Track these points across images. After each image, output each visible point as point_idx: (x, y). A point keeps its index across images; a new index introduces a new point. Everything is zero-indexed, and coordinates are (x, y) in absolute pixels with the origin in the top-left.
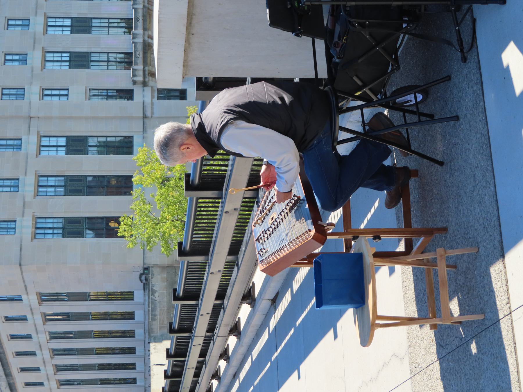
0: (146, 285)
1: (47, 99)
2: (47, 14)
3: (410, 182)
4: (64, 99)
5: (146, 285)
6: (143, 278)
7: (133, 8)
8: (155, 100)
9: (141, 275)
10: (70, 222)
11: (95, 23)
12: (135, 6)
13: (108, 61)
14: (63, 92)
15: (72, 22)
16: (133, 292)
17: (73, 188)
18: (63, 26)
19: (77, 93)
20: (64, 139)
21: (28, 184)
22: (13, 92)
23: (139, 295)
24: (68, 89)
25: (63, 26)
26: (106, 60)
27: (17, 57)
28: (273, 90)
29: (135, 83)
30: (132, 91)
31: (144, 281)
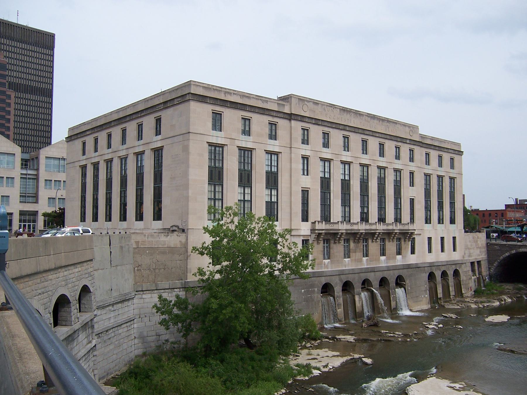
0: (171, 230)
1: (301, 161)
2: (226, 146)
3: (378, 380)
4: (301, 173)
5: (171, 230)
6: (174, 228)
7: (315, 221)
8: (302, 238)
9: (178, 227)
10: (219, 172)
11: (247, 190)
12: (317, 222)
13: (215, 200)
14: (306, 171)
15: (347, 180)
16: (142, 220)
17: (243, 175)
18: (215, 160)
19: (306, 182)
20: (276, 170)
21: (247, 142)
22: (306, 138)
23: (158, 224)
24: (308, 175)
25: (215, 160)
26: (217, 198)
27: (306, 138)
28: (511, 288)
29: (314, 223)
30: (307, 221)
31: (171, 229)
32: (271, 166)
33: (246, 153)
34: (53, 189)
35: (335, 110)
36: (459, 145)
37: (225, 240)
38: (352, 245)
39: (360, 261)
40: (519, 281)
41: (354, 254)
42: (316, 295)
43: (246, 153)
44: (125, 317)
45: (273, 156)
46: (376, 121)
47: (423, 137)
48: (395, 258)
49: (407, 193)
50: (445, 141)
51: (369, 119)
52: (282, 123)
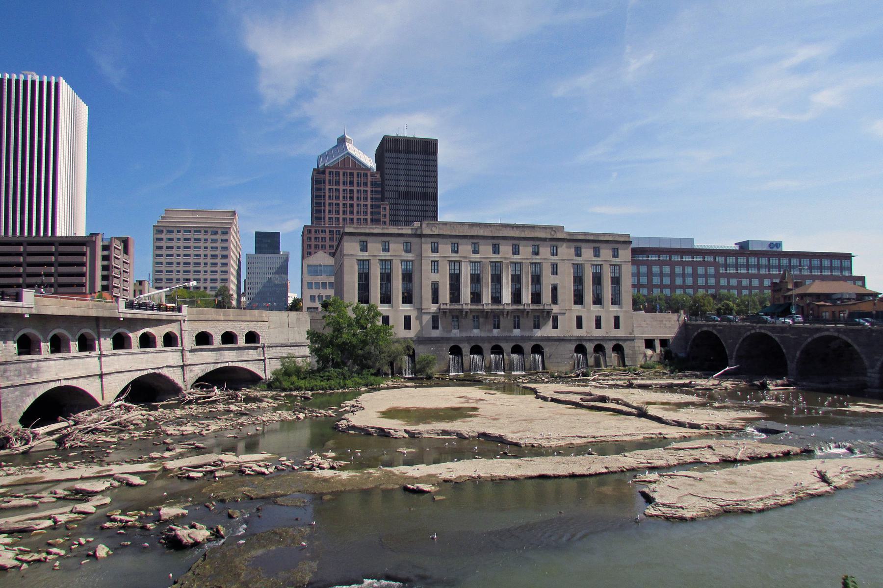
19: (435, 277)
39: (491, 331)
49: (548, 280)
52: (414, 240)
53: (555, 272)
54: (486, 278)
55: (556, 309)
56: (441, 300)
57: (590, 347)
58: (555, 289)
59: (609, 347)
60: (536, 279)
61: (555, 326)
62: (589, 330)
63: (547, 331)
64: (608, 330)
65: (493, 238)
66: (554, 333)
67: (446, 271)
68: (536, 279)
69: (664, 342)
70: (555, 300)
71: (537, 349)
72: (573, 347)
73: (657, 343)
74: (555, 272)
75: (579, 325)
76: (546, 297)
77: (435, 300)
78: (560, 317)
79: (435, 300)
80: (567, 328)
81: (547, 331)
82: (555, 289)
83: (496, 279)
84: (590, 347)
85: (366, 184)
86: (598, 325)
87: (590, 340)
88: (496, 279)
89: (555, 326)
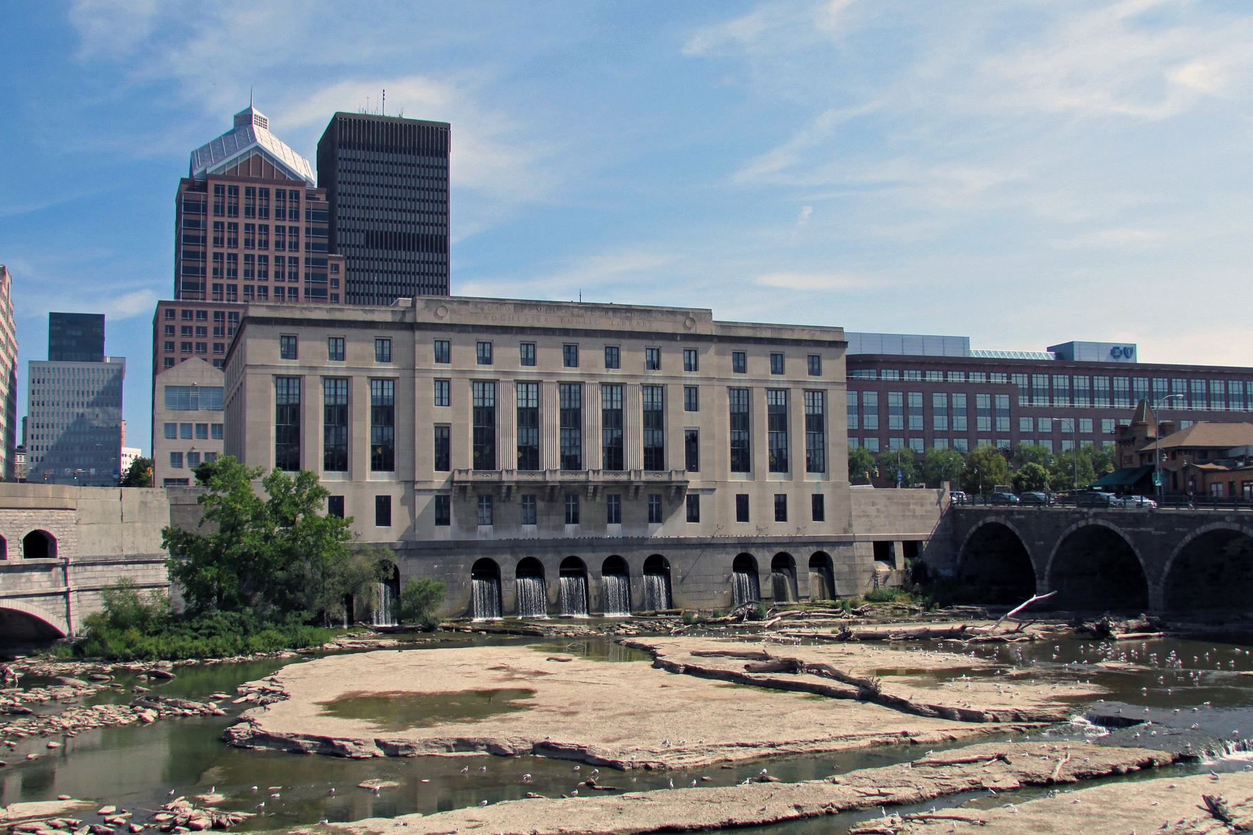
19: (443, 415)
32: (484, 398)
33: (572, 391)
34: (179, 436)
35: (504, 308)
36: (840, 330)
37: (1089, 443)
38: (540, 505)
39: (561, 528)
40: (571, 833)
41: (545, 518)
42: (461, 574)
43: (572, 391)
44: (152, 581)
45: (487, 386)
46: (597, 314)
47: (722, 325)
48: (605, 528)
49: (678, 422)
50: (792, 328)
51: (582, 311)
52: (398, 336)
53: (692, 405)
54: (551, 418)
55: (694, 481)
56: (455, 463)
57: (764, 560)
58: (692, 440)
59: (802, 558)
60: (655, 419)
61: (693, 517)
62: (762, 524)
63: (677, 526)
64: (800, 524)
65: (566, 332)
66: (691, 531)
67: (466, 399)
68: (655, 419)
69: (911, 548)
70: (692, 462)
71: (656, 565)
72: (729, 558)
73: (898, 550)
74: (692, 405)
75: (743, 515)
76: (675, 456)
77: (443, 462)
78: (702, 498)
79: (443, 462)
80: (718, 521)
81: (677, 526)
82: (692, 440)
83: (572, 419)
84: (764, 560)
85: (295, 215)
86: (781, 514)
87: (765, 545)
88: (572, 419)
89: (693, 517)
